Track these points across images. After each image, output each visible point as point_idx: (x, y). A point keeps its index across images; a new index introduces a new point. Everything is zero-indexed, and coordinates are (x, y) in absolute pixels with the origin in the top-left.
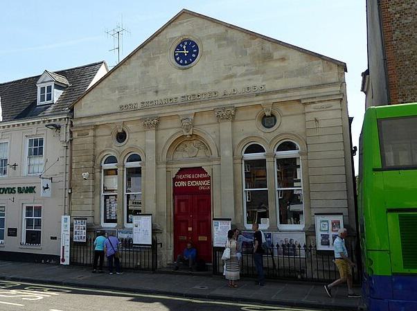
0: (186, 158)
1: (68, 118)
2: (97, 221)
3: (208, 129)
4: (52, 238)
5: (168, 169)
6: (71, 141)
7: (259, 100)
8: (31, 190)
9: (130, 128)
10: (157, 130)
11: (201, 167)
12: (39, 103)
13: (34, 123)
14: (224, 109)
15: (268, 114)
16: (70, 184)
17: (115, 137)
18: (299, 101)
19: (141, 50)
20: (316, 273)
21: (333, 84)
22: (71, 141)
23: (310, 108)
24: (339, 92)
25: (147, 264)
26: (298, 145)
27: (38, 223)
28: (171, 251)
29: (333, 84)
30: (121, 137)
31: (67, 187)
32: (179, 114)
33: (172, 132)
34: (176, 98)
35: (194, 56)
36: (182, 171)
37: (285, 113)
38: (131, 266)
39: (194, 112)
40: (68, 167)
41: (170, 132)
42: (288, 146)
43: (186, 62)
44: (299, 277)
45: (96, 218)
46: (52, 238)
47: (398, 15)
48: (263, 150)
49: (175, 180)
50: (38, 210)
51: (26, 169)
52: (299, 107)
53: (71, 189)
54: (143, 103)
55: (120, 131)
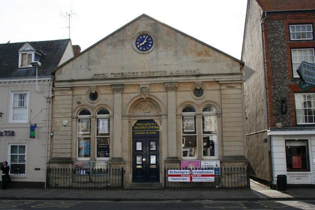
0: (144, 113)
1: (51, 80)
2: (74, 157)
3: (159, 94)
4: (36, 169)
5: (130, 121)
6: (53, 97)
8: (12, 134)
10: (122, 93)
11: (153, 120)
12: (19, 67)
13: (19, 82)
14: (171, 83)
15: (198, 88)
16: (51, 129)
17: (88, 96)
18: (218, 82)
19: (111, 37)
20: (234, 184)
21: (236, 74)
22: (53, 97)
24: (240, 79)
25: (68, 183)
26: (91, 112)
27: (22, 158)
28: (131, 176)
29: (236, 74)
30: (94, 96)
31: (50, 131)
32: (139, 83)
33: (133, 96)
34: (137, 73)
35: (150, 45)
36: (139, 121)
37: (208, 89)
38: (227, 185)
39: (150, 83)
40: (50, 116)
41: (131, 94)
43: (144, 49)
44: (217, 187)
45: (74, 153)
46: (36, 169)
47: (272, 39)
48: (108, 113)
50: (23, 148)
51: (19, 118)
52: (218, 87)
53: (53, 132)
54: (142, 72)
55: (93, 92)
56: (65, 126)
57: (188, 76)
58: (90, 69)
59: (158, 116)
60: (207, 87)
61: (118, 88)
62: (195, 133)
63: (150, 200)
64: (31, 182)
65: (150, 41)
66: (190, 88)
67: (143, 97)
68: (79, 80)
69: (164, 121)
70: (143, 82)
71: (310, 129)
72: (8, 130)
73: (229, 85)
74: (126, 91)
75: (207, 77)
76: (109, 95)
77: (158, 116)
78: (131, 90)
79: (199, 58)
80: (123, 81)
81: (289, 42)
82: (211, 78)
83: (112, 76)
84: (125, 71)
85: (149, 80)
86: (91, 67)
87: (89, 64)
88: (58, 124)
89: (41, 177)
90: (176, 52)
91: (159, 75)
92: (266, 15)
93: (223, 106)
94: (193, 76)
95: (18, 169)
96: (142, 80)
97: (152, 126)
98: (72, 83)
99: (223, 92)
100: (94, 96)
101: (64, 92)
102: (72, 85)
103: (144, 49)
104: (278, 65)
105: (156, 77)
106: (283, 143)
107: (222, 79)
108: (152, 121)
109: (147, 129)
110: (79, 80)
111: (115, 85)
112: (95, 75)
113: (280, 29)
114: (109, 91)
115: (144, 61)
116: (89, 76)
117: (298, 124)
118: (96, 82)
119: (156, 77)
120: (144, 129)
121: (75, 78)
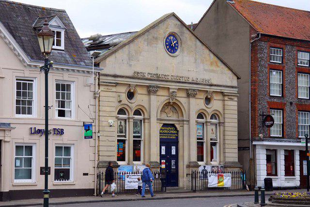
0: (171, 117)
3: (182, 99)
7: (207, 88)
9: (139, 90)
23: (226, 98)
27: (68, 162)
37: (215, 98)
39: (178, 87)
42: (137, 112)
49: (161, 129)
50: (68, 149)
55: (132, 91)
56: (111, 126)
57: (205, 85)
58: (130, 66)
59: (179, 121)
60: (215, 97)
61: (151, 90)
62: (125, 136)
63: (244, 195)
64: (80, 189)
65: (171, 51)
66: (203, 96)
67: (171, 101)
68: (123, 77)
69: (186, 126)
70: (173, 86)
71: (277, 141)
72: (57, 127)
73: (230, 97)
74: (158, 93)
75: (216, 88)
76: (144, 96)
77: (179, 121)
78: (161, 92)
79: (212, 68)
80: (158, 83)
81: (269, 63)
82: (218, 89)
83: (149, 77)
84: (160, 72)
85: (178, 84)
86: (132, 63)
87: (129, 59)
88: (104, 124)
89: (89, 183)
90: (196, 60)
91: (184, 81)
92: (260, 36)
93: (226, 116)
94: (208, 85)
95: (62, 175)
96: (173, 84)
97: (172, 130)
98: (117, 79)
99: (226, 103)
100: (131, 95)
101: (110, 88)
102: (115, 81)
103: (170, 50)
104: (263, 83)
105: (183, 83)
106: (265, 152)
107: (226, 90)
108: (173, 125)
109: (168, 133)
110: (123, 77)
111: (154, 86)
112: (135, 72)
113: (265, 51)
114: (220, 97)
115: (173, 65)
116: (130, 74)
117: (271, 136)
118: (137, 81)
119: (183, 83)
120: (166, 133)
121: (118, 73)
